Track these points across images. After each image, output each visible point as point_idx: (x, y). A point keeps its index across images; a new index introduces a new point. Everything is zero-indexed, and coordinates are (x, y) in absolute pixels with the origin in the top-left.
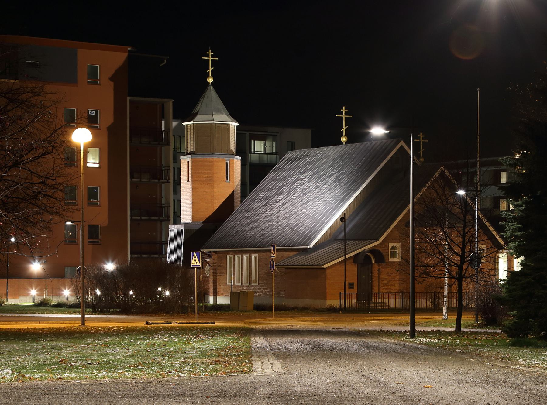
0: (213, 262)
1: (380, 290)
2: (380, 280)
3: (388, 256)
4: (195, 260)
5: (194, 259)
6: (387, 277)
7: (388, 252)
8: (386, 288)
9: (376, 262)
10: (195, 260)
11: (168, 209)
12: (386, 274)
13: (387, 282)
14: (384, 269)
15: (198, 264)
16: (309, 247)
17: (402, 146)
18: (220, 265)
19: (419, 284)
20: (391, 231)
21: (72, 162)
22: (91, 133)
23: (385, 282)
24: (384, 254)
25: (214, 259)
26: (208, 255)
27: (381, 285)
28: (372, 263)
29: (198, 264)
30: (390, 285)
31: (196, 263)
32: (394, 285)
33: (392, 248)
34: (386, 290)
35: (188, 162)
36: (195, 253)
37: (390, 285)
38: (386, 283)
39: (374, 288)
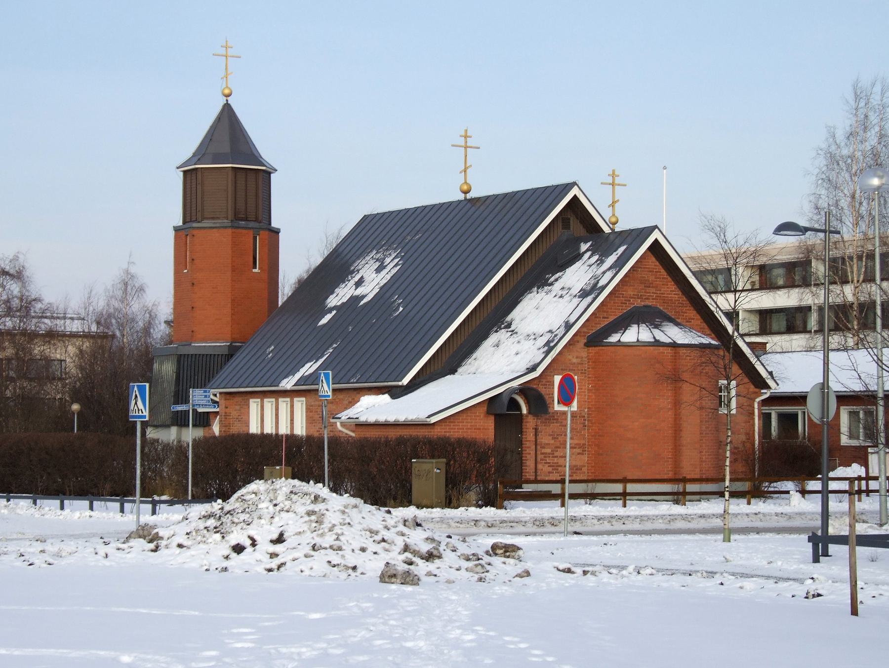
0: (226, 413)
1: (819, 508)
2: (539, 447)
3: (553, 401)
4: (136, 403)
5: (133, 402)
6: (553, 442)
9: (530, 412)
10: (136, 403)
12: (550, 435)
14: (544, 426)
15: (142, 413)
16: (400, 383)
17: (575, 195)
18: (237, 418)
20: (560, 353)
21: (517, 488)
22: (523, 502)
23: (548, 451)
24: (546, 397)
26: (205, 402)
27: (540, 457)
29: (142, 413)
31: (139, 410)
34: (549, 466)
36: (136, 387)
38: (549, 454)
39: (526, 463)
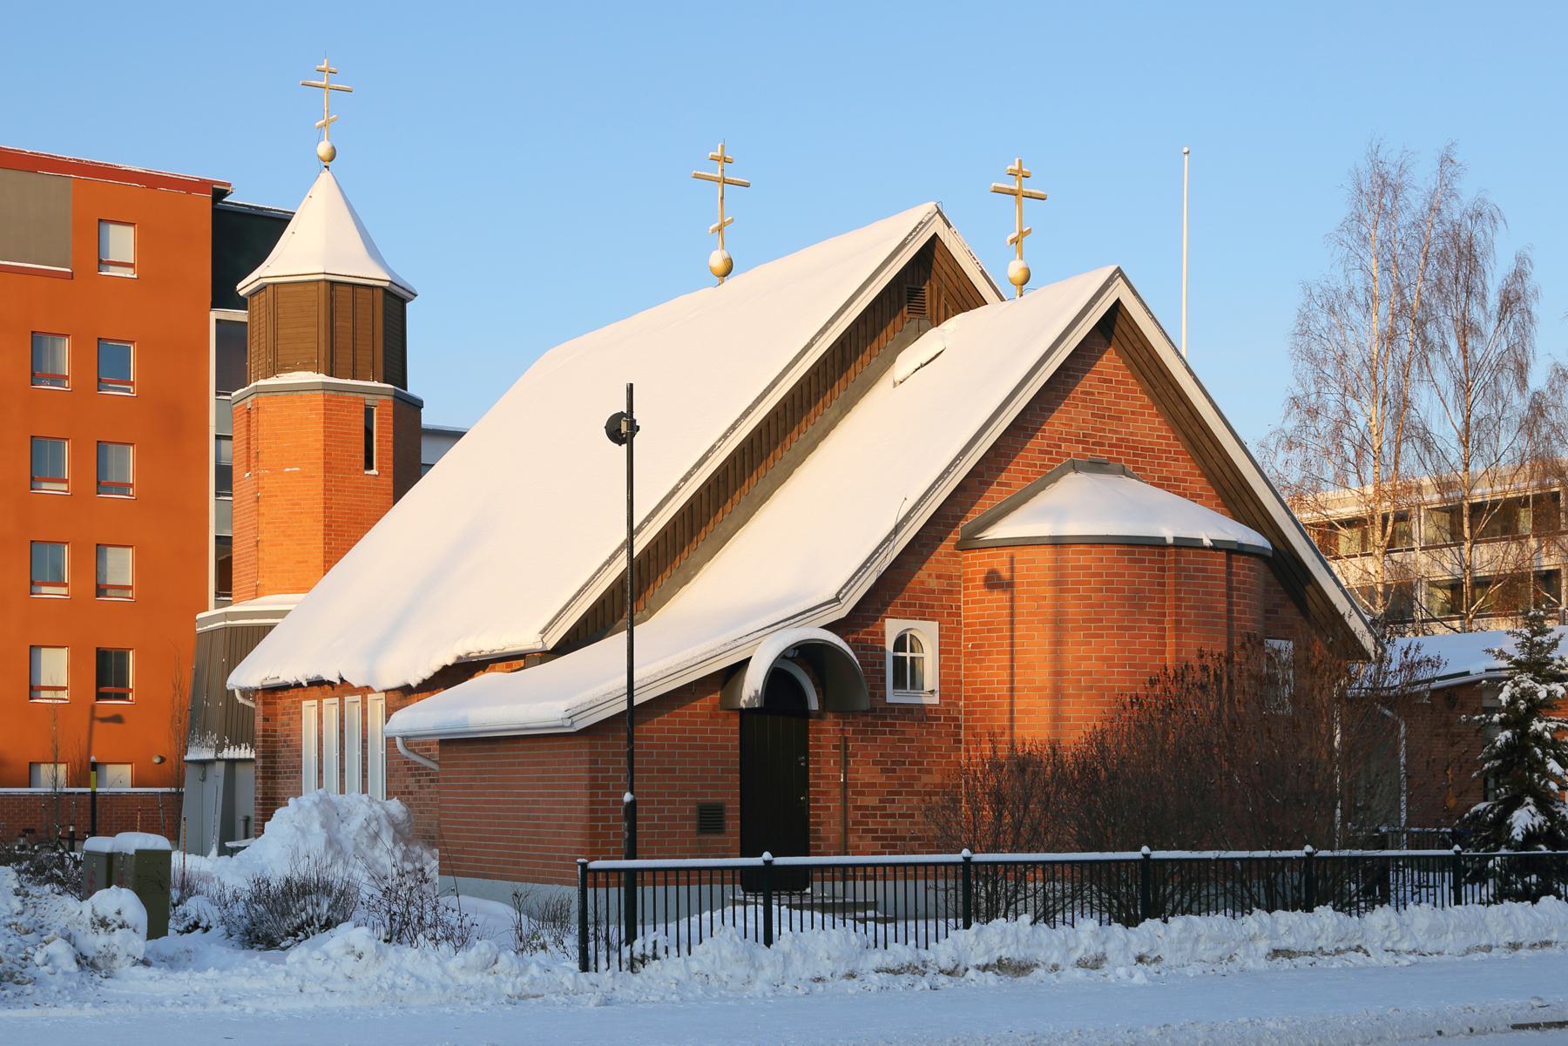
3: (883, 679)
7: (883, 664)
8: (876, 831)
11: (865, 885)
13: (880, 801)
19: (17, 895)
23: (873, 801)
25: (268, 720)
27: (855, 815)
28: (806, 714)
30: (892, 816)
32: (912, 816)
33: (900, 644)
35: (369, 412)
37: (892, 816)
